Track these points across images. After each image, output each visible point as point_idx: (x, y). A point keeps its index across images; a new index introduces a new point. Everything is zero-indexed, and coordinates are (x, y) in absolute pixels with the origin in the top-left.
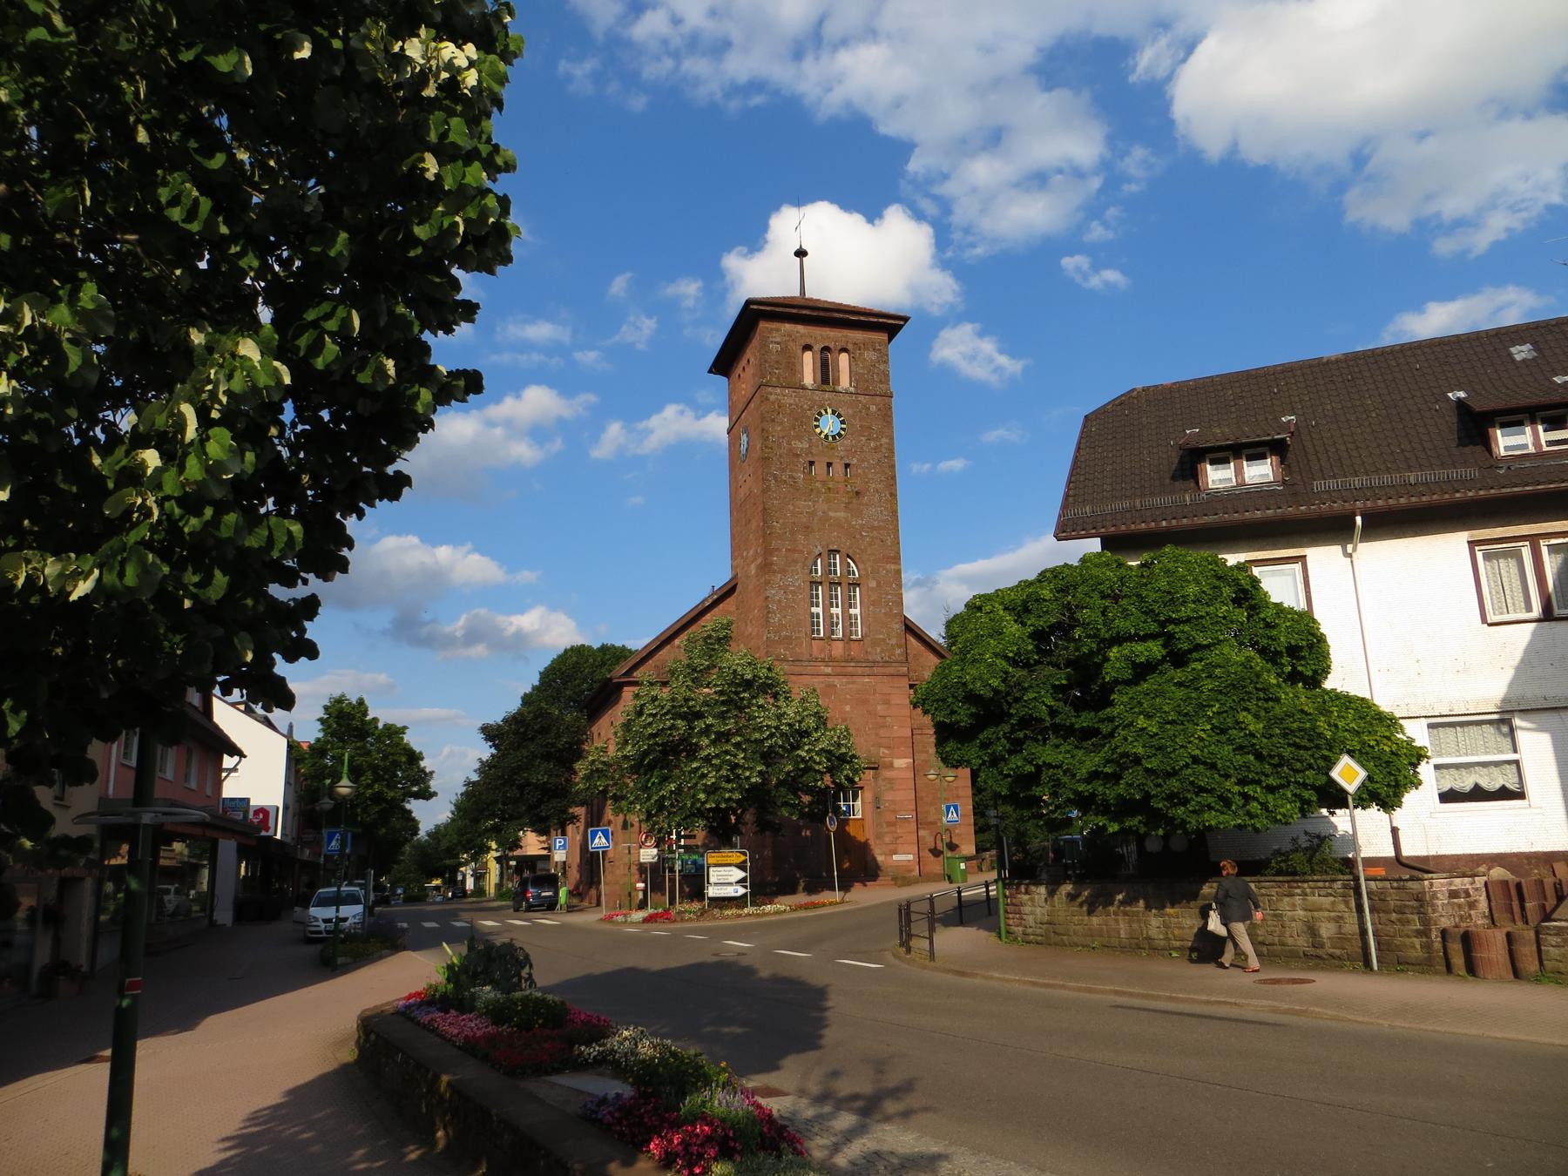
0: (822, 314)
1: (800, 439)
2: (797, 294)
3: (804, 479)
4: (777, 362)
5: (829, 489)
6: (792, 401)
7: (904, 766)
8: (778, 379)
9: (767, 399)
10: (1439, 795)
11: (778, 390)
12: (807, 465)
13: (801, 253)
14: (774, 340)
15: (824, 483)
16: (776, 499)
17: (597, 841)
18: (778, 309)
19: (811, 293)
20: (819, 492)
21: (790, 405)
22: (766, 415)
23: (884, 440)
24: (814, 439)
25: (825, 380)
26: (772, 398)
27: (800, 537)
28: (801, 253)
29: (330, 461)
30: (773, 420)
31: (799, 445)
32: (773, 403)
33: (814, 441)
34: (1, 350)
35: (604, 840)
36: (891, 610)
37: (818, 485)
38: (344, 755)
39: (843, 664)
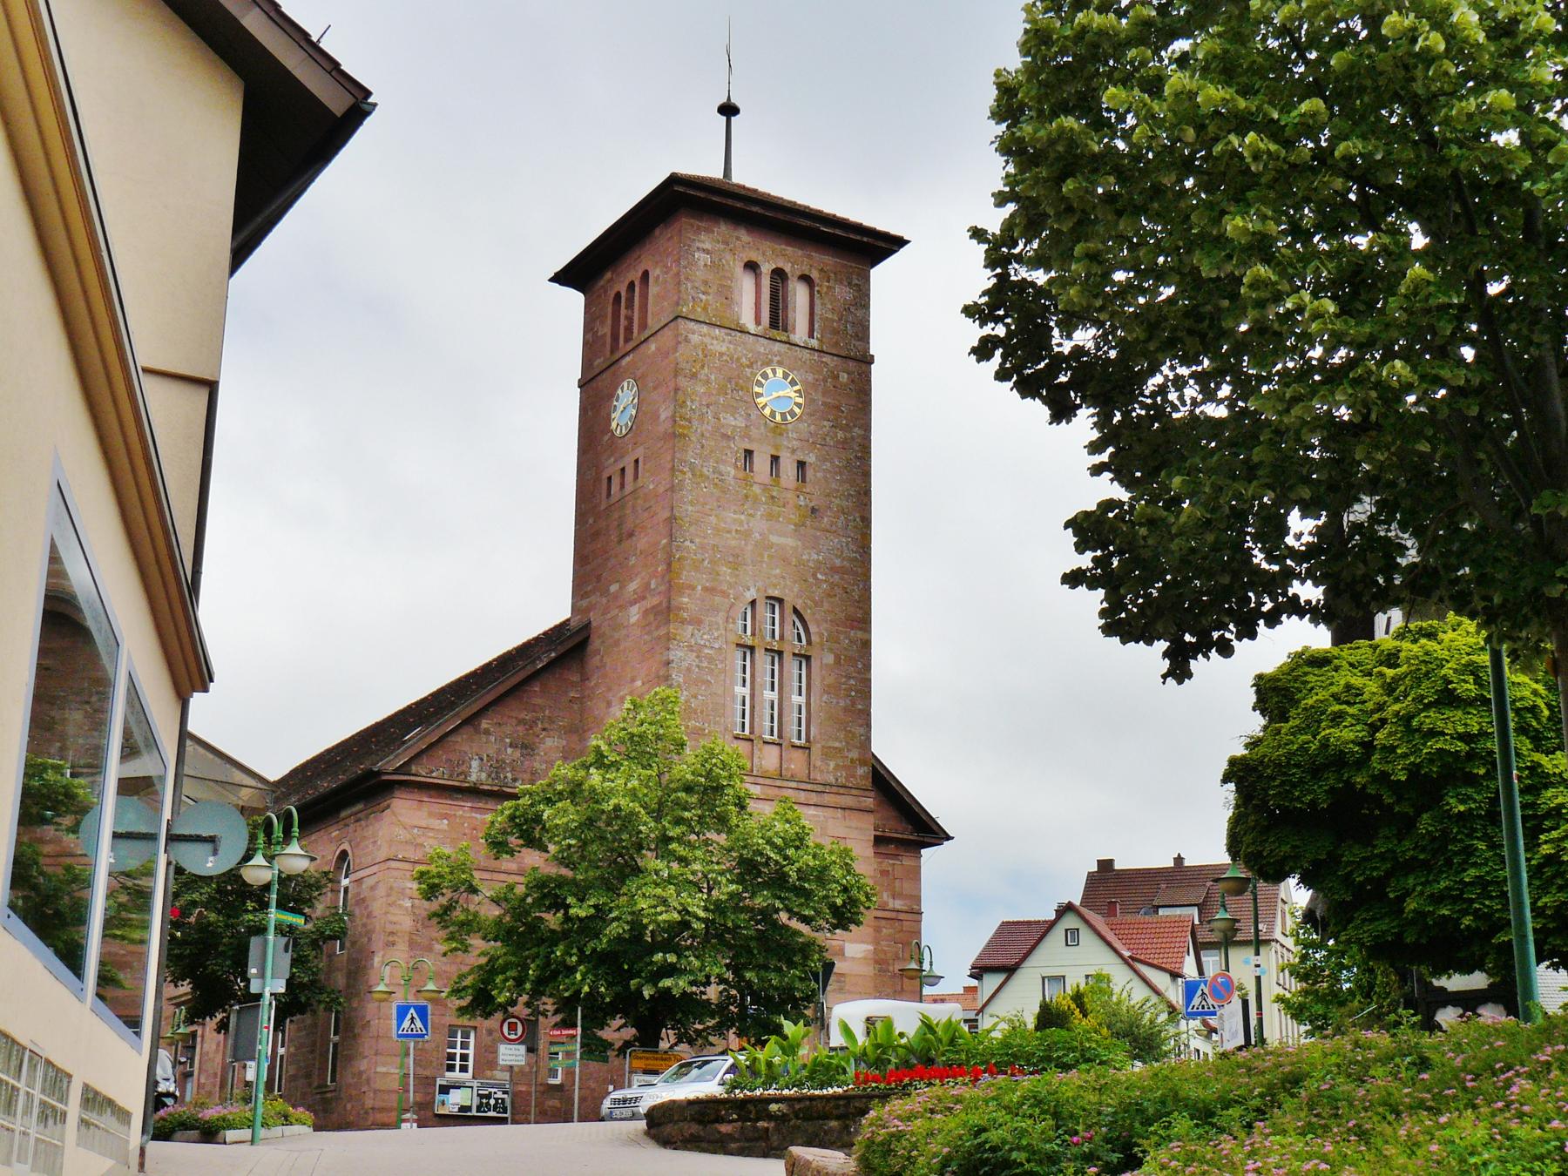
0: (781, 216)
1: (734, 411)
2: (721, 176)
3: (735, 478)
4: (706, 283)
5: (773, 497)
6: (724, 349)
7: (859, 955)
8: (705, 309)
9: (687, 340)
10: (150, 777)
11: (705, 329)
12: (741, 455)
13: (728, 110)
14: (701, 245)
15: (765, 487)
16: (691, 503)
17: (406, 1024)
18: (730, 202)
19: (738, 178)
20: (756, 500)
21: (721, 354)
22: (683, 365)
23: (857, 431)
24: (754, 414)
25: (774, 324)
26: (695, 338)
27: (725, 570)
28: (728, 110)
29: (1515, 434)
30: (694, 376)
31: (733, 421)
32: (695, 347)
33: (753, 417)
34: (1155, 2)
35: (419, 1024)
36: (853, 704)
37: (756, 489)
38: (150, 873)
39: (778, 783)
